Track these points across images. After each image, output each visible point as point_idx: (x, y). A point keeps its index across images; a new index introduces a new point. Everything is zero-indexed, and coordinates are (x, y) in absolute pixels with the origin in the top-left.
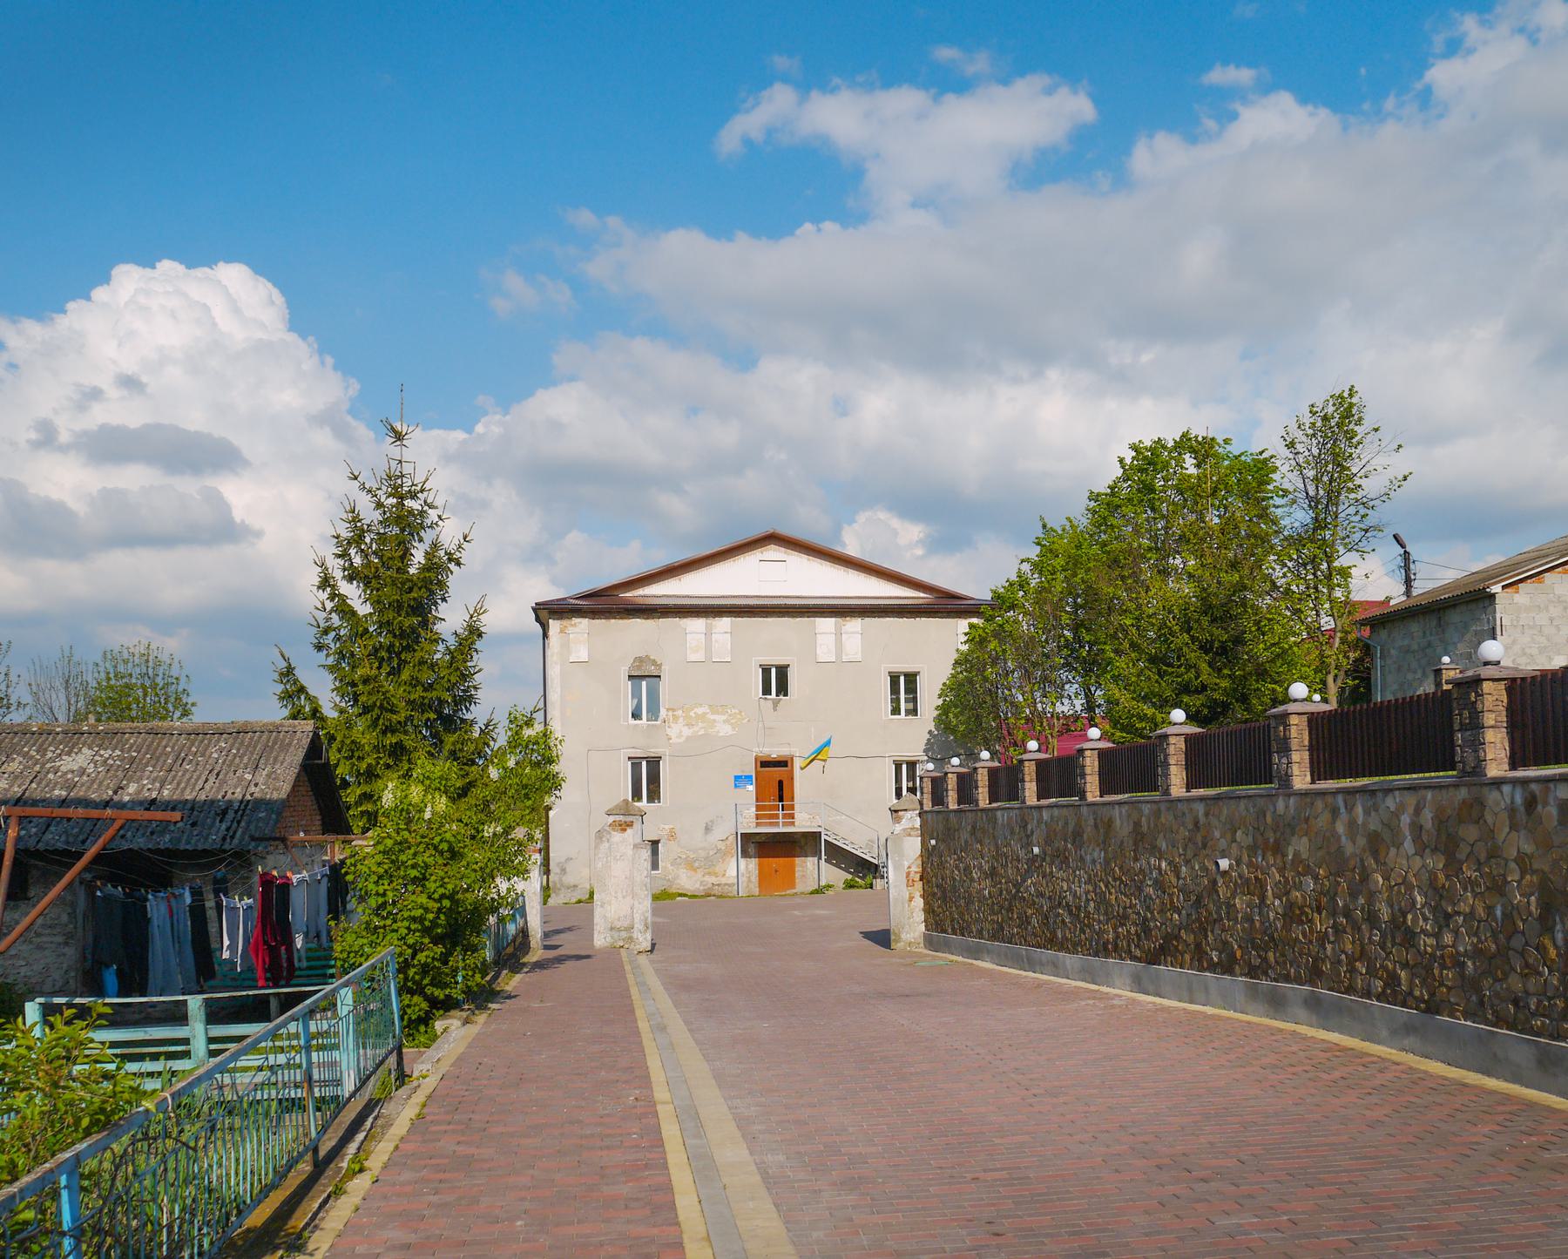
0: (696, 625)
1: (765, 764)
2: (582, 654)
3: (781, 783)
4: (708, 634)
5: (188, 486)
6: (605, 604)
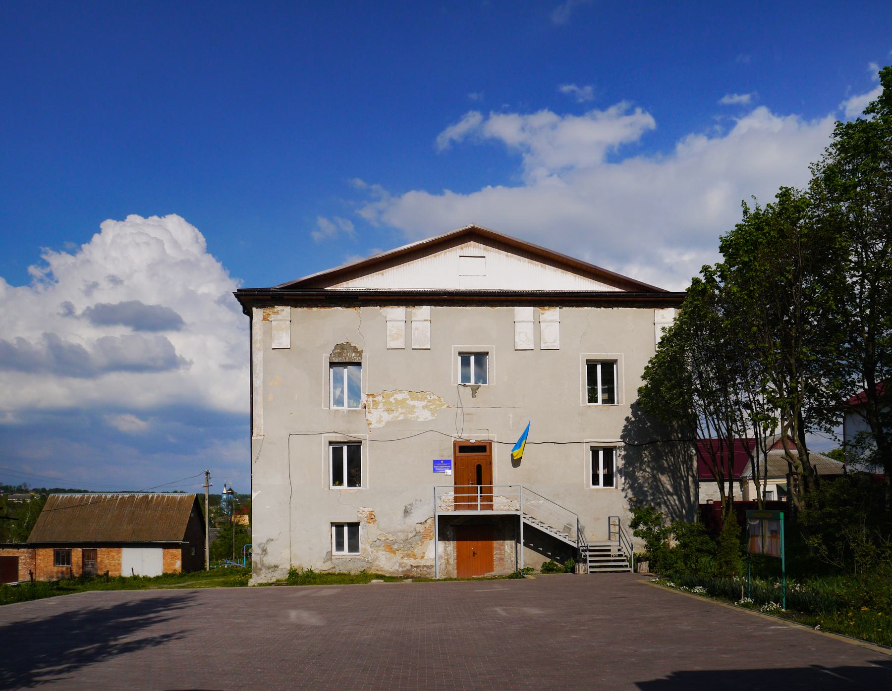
0: (397, 313)
1: (463, 448)
2: (284, 340)
3: (479, 467)
4: (408, 322)
5: (149, 337)
6: (310, 294)
